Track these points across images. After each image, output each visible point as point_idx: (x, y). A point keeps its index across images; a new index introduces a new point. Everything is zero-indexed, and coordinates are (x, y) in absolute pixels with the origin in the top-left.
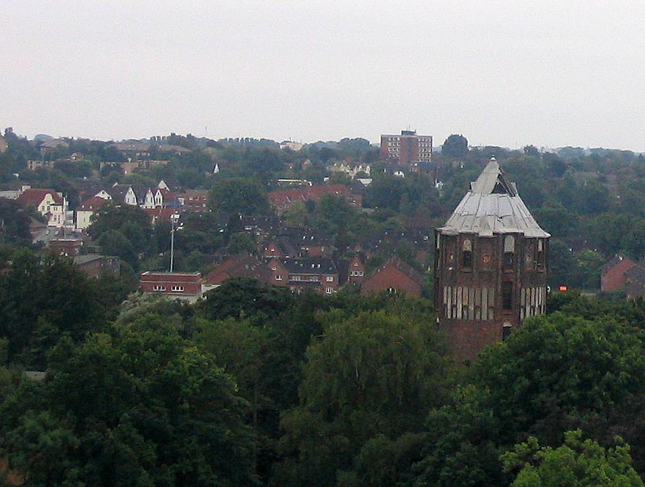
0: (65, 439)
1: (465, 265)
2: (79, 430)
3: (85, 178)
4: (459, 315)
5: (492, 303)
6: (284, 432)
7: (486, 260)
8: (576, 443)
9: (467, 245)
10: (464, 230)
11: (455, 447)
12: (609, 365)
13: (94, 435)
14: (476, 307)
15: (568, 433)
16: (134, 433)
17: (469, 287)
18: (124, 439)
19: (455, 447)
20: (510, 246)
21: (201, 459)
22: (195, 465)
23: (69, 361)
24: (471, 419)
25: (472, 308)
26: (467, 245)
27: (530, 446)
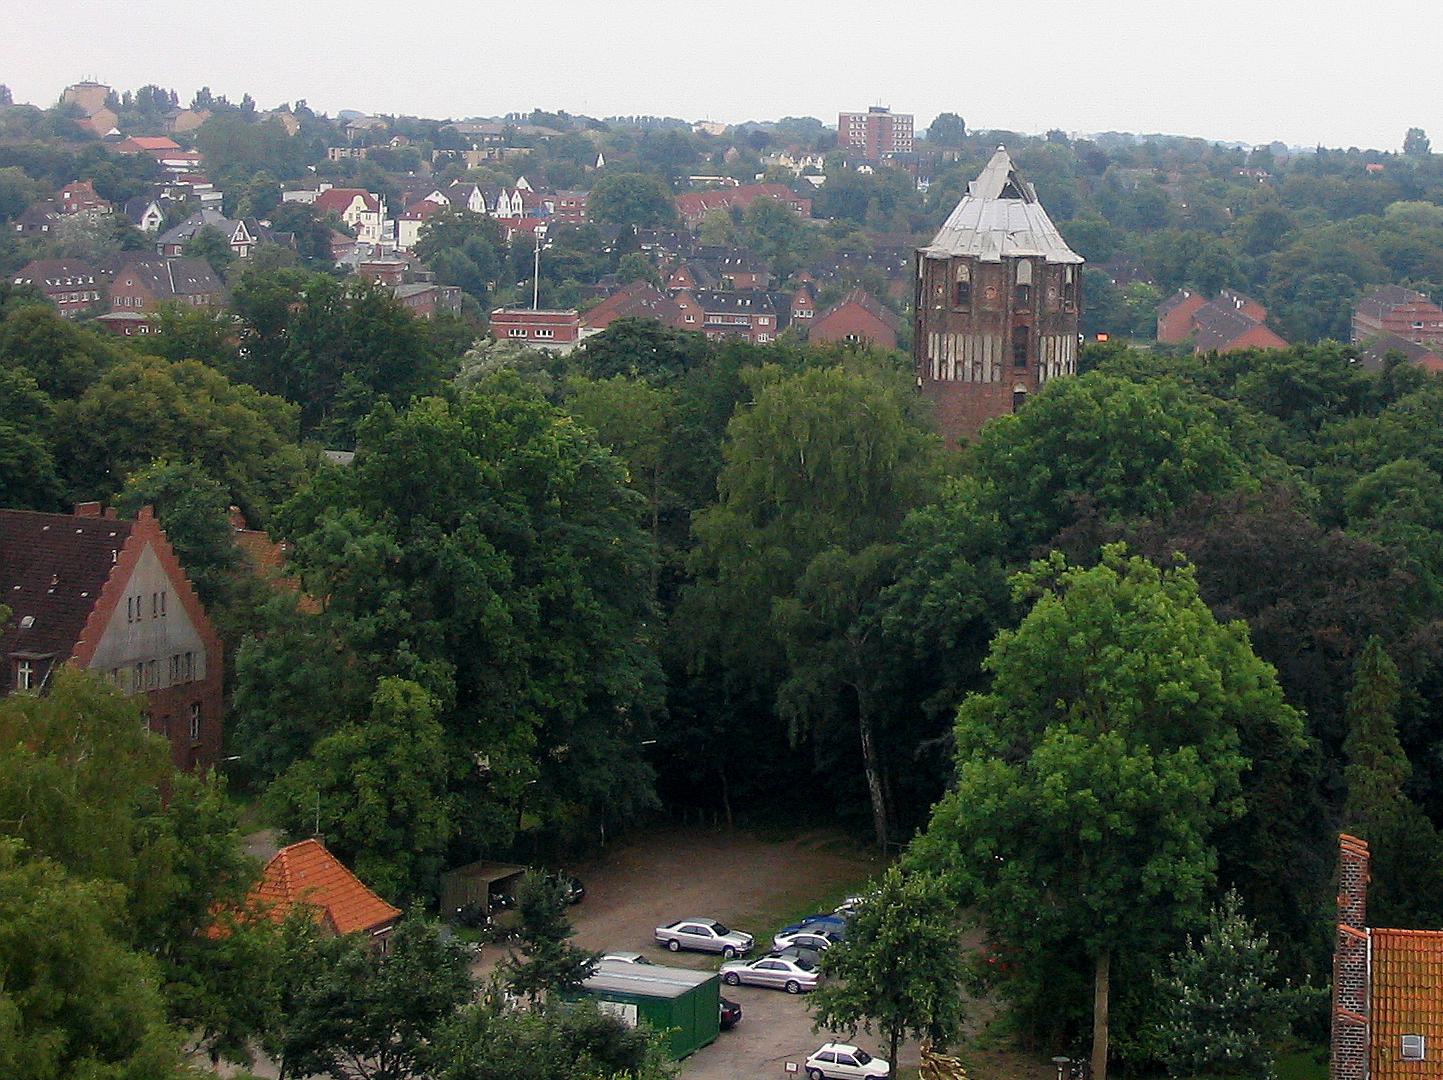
4: (951, 375)
5: (998, 358)
9: (963, 274)
12: (1167, 450)
13: (423, 542)
18: (468, 549)
22: (568, 588)
23: (387, 437)
24: (966, 525)
25: (968, 364)
27: (1052, 565)
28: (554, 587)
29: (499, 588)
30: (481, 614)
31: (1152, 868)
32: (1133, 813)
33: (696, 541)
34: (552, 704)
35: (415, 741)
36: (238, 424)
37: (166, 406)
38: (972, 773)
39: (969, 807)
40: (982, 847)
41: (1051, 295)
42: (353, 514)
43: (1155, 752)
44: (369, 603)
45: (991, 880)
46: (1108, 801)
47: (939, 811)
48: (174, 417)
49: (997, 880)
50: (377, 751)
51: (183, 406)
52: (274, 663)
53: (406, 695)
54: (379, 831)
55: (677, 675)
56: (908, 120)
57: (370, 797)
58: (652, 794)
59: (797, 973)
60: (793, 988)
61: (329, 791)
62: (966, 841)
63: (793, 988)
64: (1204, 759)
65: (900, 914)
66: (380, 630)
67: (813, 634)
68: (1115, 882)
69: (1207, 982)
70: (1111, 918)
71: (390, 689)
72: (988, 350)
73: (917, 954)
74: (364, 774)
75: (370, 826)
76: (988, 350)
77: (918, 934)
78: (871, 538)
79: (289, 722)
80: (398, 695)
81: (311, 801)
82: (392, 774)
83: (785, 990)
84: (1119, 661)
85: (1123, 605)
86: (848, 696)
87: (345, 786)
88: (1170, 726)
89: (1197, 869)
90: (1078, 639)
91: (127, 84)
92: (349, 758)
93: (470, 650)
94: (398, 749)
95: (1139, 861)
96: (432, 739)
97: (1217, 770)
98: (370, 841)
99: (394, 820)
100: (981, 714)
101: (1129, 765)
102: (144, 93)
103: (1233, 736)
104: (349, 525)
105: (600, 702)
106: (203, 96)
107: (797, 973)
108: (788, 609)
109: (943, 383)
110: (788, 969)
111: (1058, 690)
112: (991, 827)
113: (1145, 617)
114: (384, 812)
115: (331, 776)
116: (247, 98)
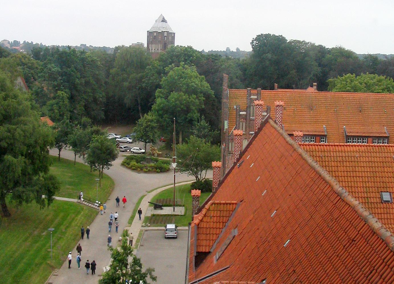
0: (58, 71)
1: (155, 39)
2: (62, 68)
3: (43, 196)
4: (153, 51)
5: (161, 48)
6: (111, 74)
7: (160, 38)
8: (183, 66)
9: (155, 34)
10: (154, 31)
11: (153, 75)
12: (191, 56)
13: (65, 70)
14: (157, 49)
15: (181, 63)
16: (75, 70)
17: (156, 44)
18: (72, 71)
19: (153, 75)
20: (165, 34)
21: (91, 78)
22: (90, 79)
23: (59, 53)
24: (157, 68)
25: (156, 49)
26: (155, 34)
27: (172, 66)
28: (88, 79)
29: (78, 78)
30: (75, 82)
31: (189, 115)
32: (185, 106)
33: (111, 74)
34: (87, 98)
35: (64, 102)
36: (33, 63)
37: (20, 61)
38: (158, 101)
39: (159, 106)
40: (160, 112)
41: (170, 38)
42: (53, 65)
43: (189, 95)
44: (55, 79)
45: (162, 118)
46: (181, 104)
47: (153, 107)
48: (22, 62)
49: (163, 118)
50: (57, 104)
51: (23, 60)
52: (39, 90)
53: (62, 94)
54: (58, 117)
55: (108, 98)
56: (142, 45)
57: (56, 111)
58: (104, 116)
59: (129, 140)
60: (128, 142)
61: (49, 110)
62: (158, 111)
63: (128, 142)
64: (197, 98)
65: (147, 122)
66: (58, 84)
67: (129, 88)
68: (183, 118)
69: (199, 130)
70: (182, 124)
71: (60, 93)
72: (159, 47)
73: (150, 129)
74: (55, 107)
75: (56, 116)
76: (159, 47)
77: (150, 125)
78: (140, 73)
79: (42, 100)
80: (61, 94)
81: (47, 112)
82: (60, 108)
83: (127, 143)
84: (183, 81)
85: (183, 73)
86: (136, 100)
87: (52, 110)
88: (192, 91)
89: (196, 115)
90: (176, 78)
91: (11, 40)
92: (52, 105)
93: (73, 87)
94: (61, 103)
95: (187, 115)
96: (67, 102)
97: (200, 100)
98: (56, 119)
99: (60, 115)
100: (160, 92)
101: (184, 97)
102: (15, 41)
103: (202, 95)
104: (52, 66)
105: (95, 100)
106: (25, 42)
107: (129, 140)
108: (126, 84)
109: (152, 53)
110: (127, 139)
111: (173, 87)
112: (162, 109)
113: (187, 74)
114: (58, 114)
115: (50, 108)
116: (32, 42)
